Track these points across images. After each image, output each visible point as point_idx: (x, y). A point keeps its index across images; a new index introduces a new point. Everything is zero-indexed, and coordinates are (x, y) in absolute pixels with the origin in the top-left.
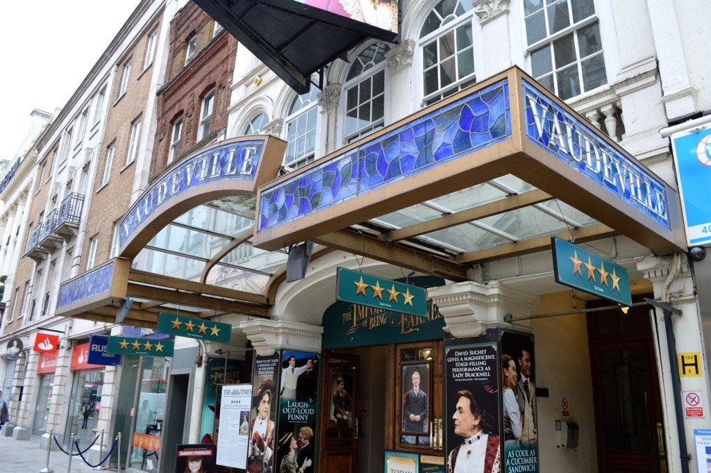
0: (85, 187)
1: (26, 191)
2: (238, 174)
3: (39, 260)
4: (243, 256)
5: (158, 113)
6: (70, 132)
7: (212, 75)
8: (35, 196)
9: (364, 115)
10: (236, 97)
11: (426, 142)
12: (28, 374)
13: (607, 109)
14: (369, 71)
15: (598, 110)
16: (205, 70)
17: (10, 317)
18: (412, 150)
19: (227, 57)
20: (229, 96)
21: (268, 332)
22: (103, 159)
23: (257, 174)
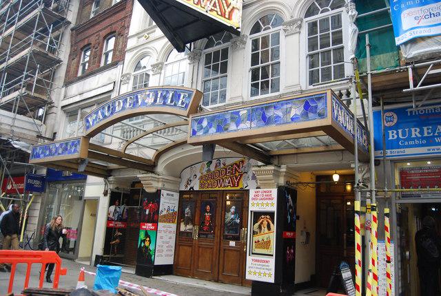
2: (175, 105)
5: (71, 42)
7: (114, 26)
9: (215, 68)
10: (131, 43)
11: (287, 112)
13: (344, 92)
14: (218, 47)
15: (340, 91)
16: (107, 22)
18: (279, 113)
19: (125, 17)
20: (126, 42)
21: (155, 180)
23: (189, 108)
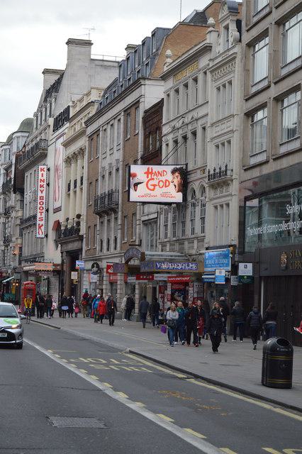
12: (104, 282)
17: (87, 245)
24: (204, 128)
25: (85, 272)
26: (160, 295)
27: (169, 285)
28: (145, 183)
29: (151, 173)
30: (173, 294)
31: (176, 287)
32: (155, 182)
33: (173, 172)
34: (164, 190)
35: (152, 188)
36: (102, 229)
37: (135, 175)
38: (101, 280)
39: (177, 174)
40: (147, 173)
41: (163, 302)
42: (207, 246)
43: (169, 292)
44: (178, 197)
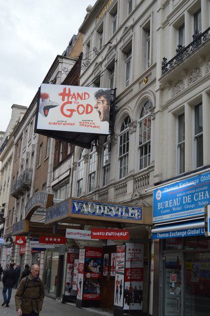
0: (33, 165)
1: (11, 158)
3: (18, 198)
4: (142, 186)
6: (26, 131)
8: (14, 162)
12: (15, 255)
17: (7, 225)
22: (39, 151)
24: (147, 30)
25: (4, 247)
26: (69, 265)
27: (82, 252)
28: (59, 108)
29: (69, 95)
30: (86, 263)
31: (91, 253)
32: (73, 106)
33: (98, 95)
34: (85, 117)
35: (68, 113)
36: (17, 211)
37: (46, 96)
38: (13, 253)
39: (102, 98)
40: (63, 95)
41: (72, 274)
42: (157, 180)
43: (81, 260)
44: (103, 128)
